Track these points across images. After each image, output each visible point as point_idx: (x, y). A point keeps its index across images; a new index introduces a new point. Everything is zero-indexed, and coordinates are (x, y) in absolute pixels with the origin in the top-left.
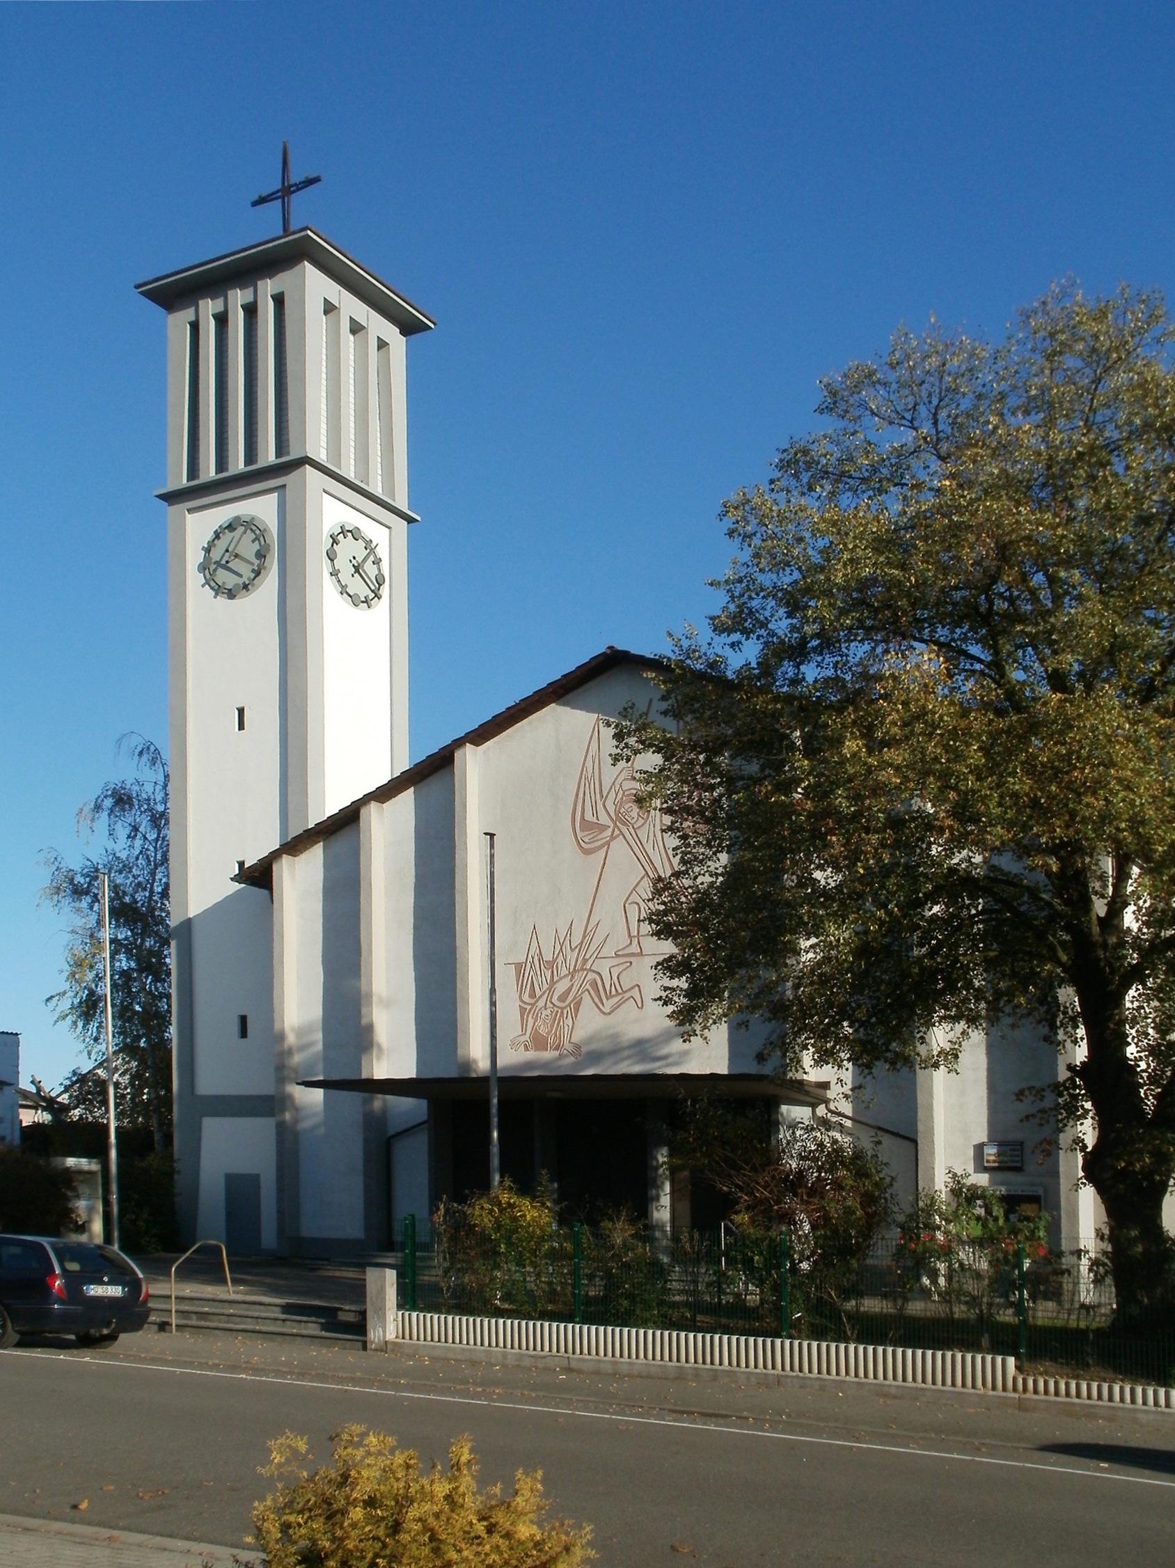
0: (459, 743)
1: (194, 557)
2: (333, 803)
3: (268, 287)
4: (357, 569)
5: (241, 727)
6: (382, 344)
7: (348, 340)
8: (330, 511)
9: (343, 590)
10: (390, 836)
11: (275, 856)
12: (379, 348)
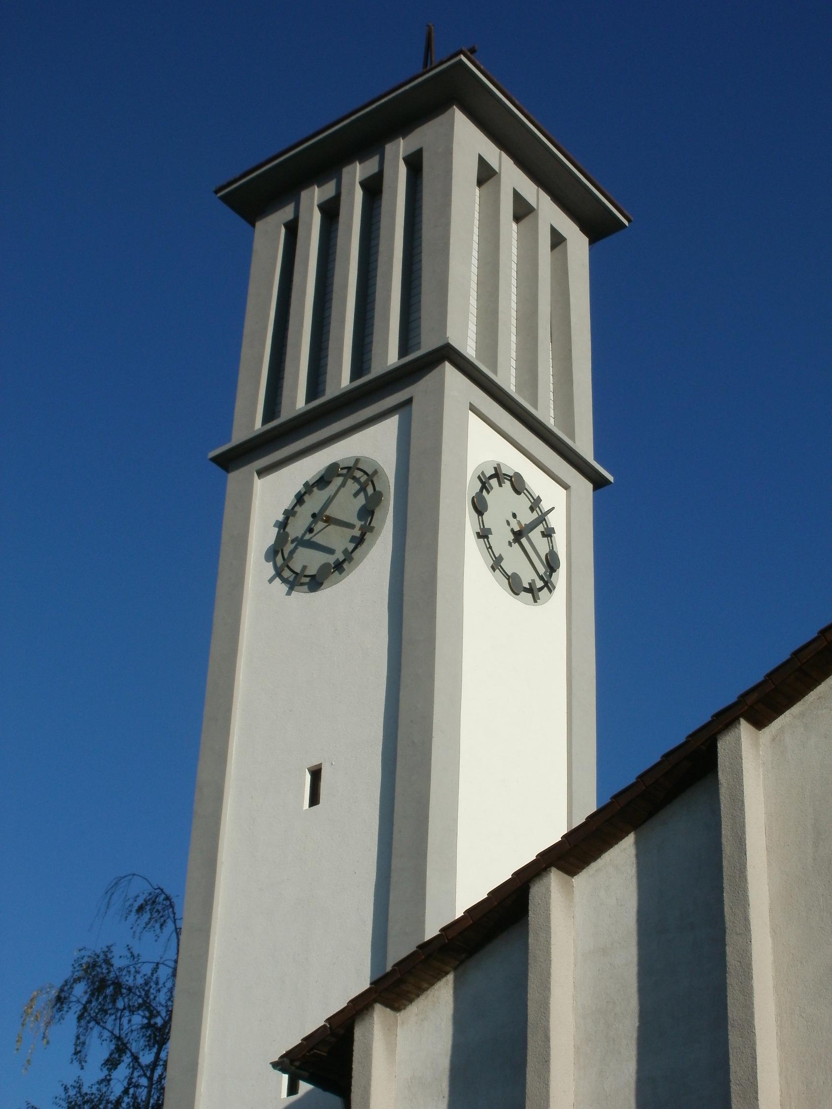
0: (724, 720)
1: (261, 535)
2: (469, 879)
3: (399, 149)
4: (518, 535)
5: (314, 800)
6: (557, 240)
7: (510, 231)
8: (480, 444)
9: (497, 564)
10: (588, 937)
11: (359, 1007)
12: (554, 246)
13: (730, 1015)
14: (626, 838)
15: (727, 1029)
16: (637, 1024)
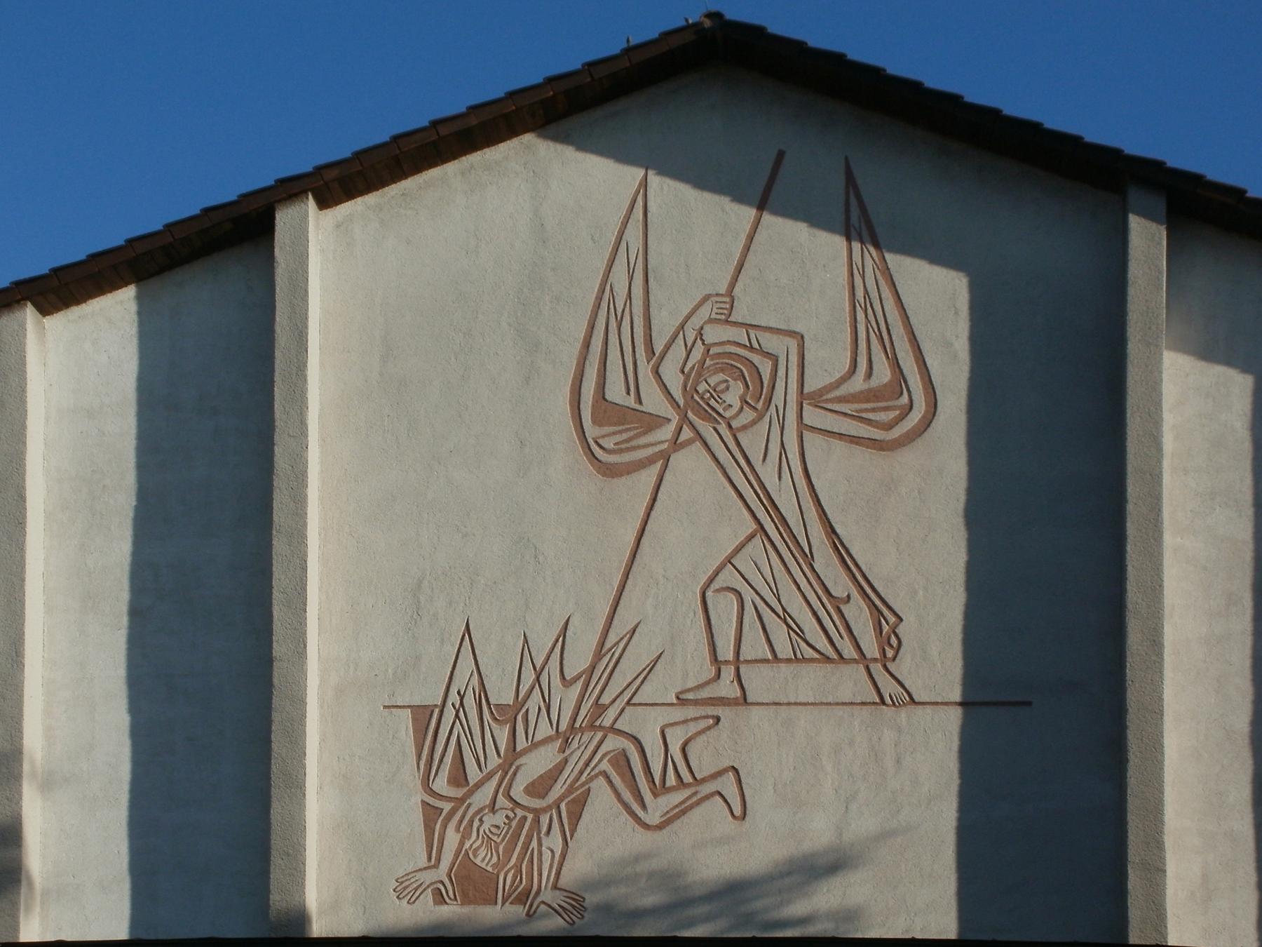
0: (292, 188)
13: (275, 518)
14: (124, 289)
15: (271, 534)
16: (134, 503)
